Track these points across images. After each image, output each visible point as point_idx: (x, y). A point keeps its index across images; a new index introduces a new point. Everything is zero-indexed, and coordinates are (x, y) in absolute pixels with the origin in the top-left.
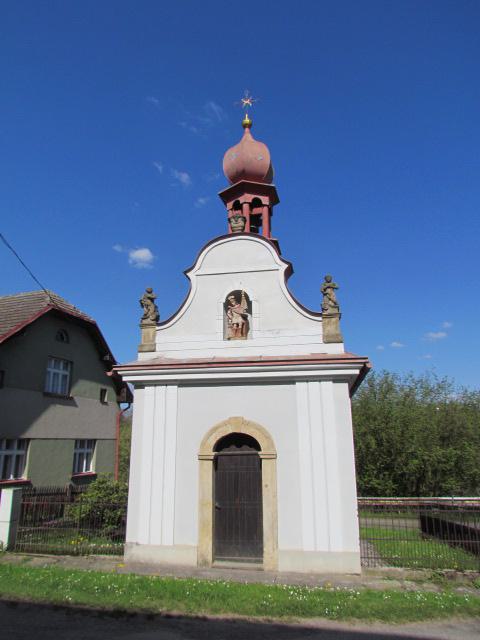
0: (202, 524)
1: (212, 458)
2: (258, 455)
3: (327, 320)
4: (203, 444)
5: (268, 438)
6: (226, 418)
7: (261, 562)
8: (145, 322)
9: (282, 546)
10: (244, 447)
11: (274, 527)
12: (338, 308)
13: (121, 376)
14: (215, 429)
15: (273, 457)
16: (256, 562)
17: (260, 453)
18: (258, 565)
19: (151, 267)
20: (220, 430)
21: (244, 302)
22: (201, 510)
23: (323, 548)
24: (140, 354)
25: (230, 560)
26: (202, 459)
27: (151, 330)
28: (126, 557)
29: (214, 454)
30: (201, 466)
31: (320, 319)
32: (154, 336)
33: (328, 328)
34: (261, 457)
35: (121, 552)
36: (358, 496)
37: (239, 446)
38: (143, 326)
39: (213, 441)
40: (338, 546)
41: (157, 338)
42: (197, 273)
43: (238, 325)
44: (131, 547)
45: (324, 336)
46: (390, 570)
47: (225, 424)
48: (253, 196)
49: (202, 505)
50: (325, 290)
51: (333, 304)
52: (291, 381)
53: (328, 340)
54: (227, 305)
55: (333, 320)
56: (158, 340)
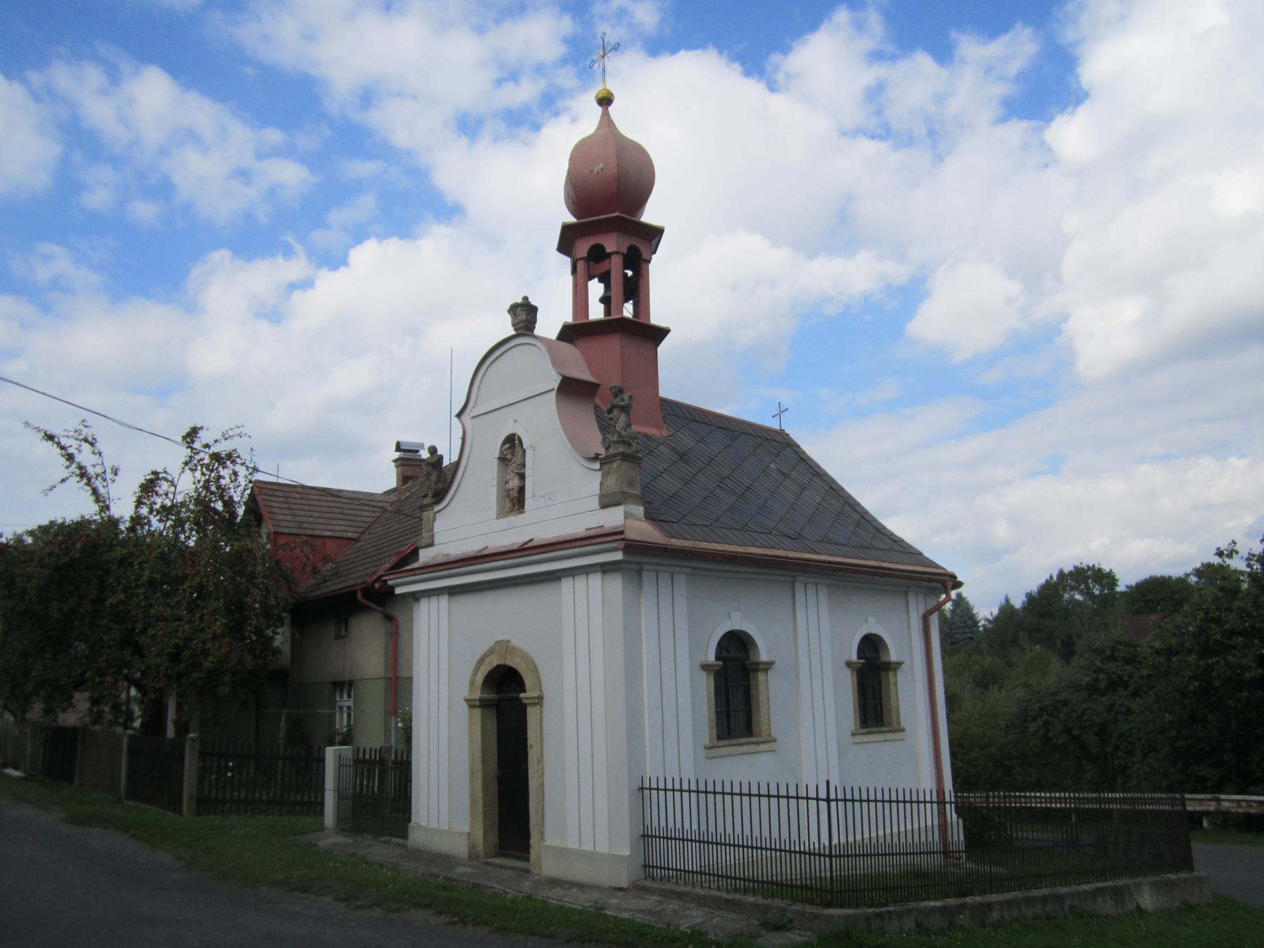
2: (519, 699)
4: (472, 683)
7: (527, 859)
9: (551, 840)
12: (100, 454)
13: (392, 588)
15: (539, 700)
16: (518, 858)
17: (522, 695)
20: (487, 661)
22: (541, 786)
23: (588, 847)
25: (512, 857)
30: (471, 715)
34: (525, 701)
42: (472, 415)
45: (601, 497)
46: (848, 917)
52: (553, 577)
53: (607, 502)
55: (615, 465)
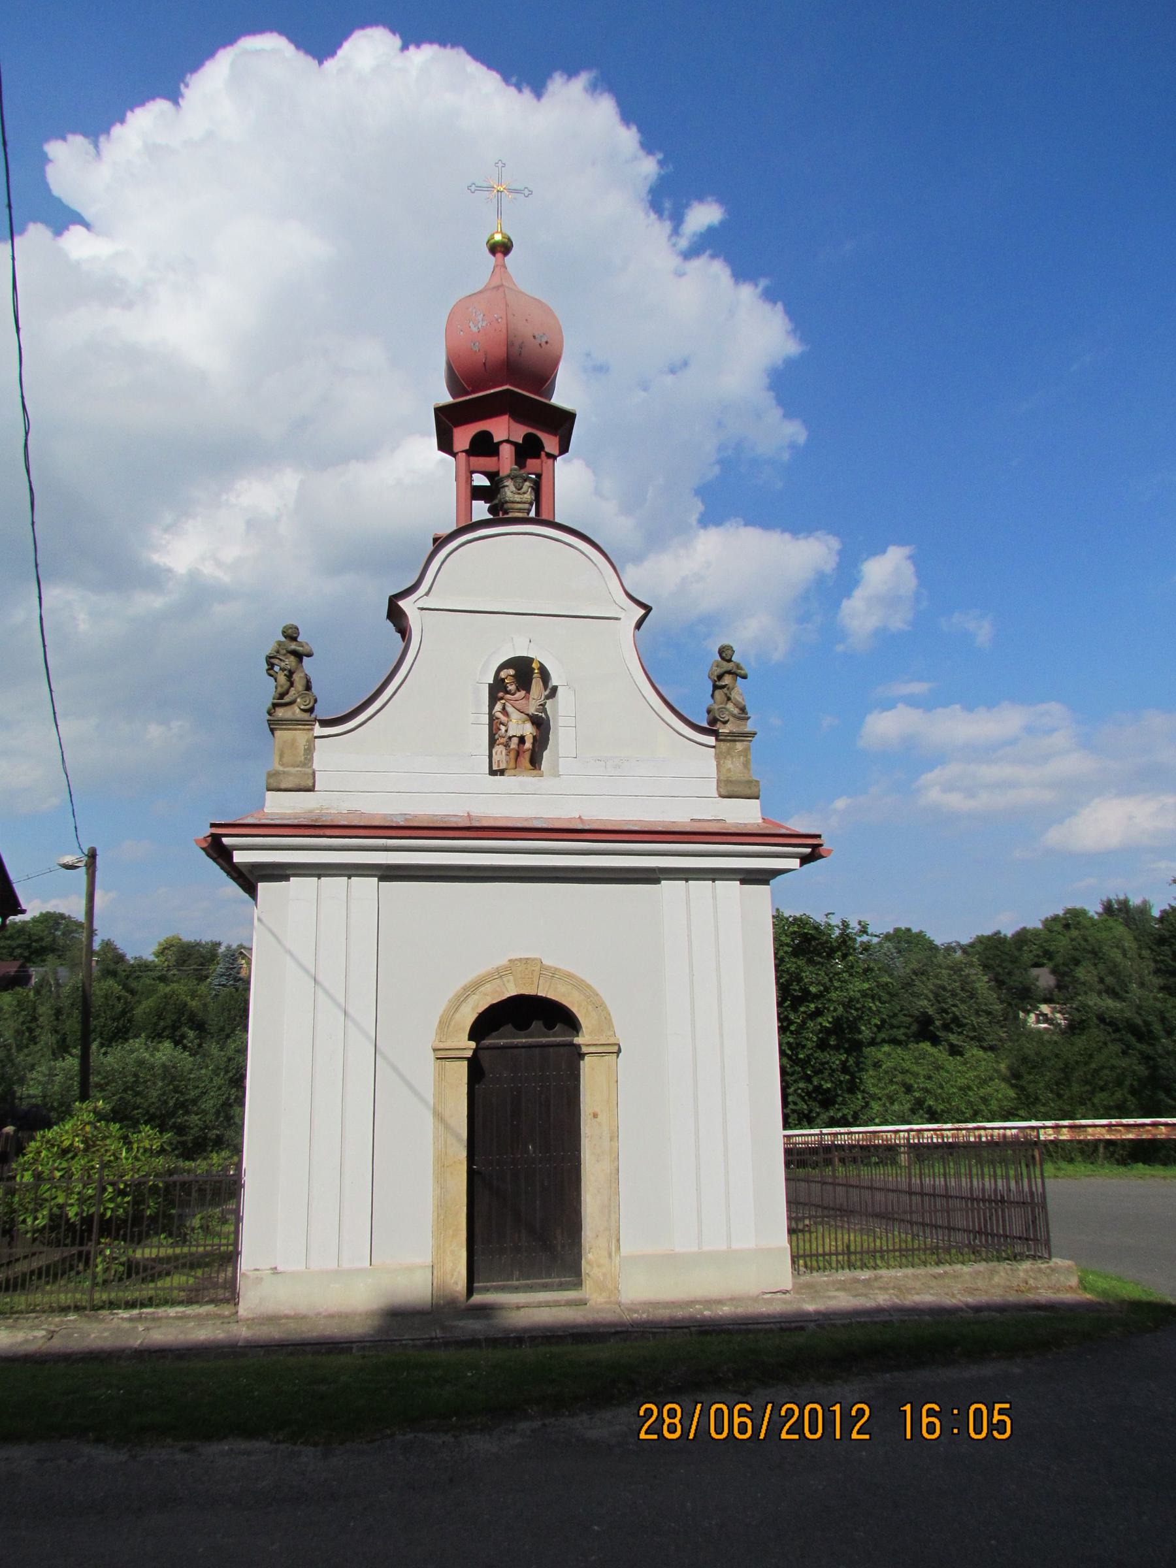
0: (442, 1206)
1: (469, 1054)
3: (724, 746)
4: (445, 1024)
5: (599, 1005)
6: (503, 961)
8: (280, 713)
10: (536, 1025)
11: (612, 1207)
14: (475, 986)
16: (562, 1287)
18: (571, 1295)
19: (1096, 917)
20: (488, 987)
21: (536, 684)
24: (270, 795)
26: (443, 1056)
27: (300, 737)
28: (244, 1309)
29: (473, 1044)
30: (440, 1078)
31: (711, 740)
32: (310, 750)
33: (729, 764)
35: (232, 1297)
36: (786, 1125)
37: (522, 1025)
38: (274, 725)
39: (468, 1015)
40: (745, 1241)
41: (316, 756)
42: (421, 604)
43: (522, 740)
44: (260, 1280)
47: (500, 973)
48: (530, 430)
49: (442, 1166)
50: (720, 677)
51: (736, 711)
52: (296, 729)
53: (731, 790)
54: (497, 689)
56: (320, 761)
